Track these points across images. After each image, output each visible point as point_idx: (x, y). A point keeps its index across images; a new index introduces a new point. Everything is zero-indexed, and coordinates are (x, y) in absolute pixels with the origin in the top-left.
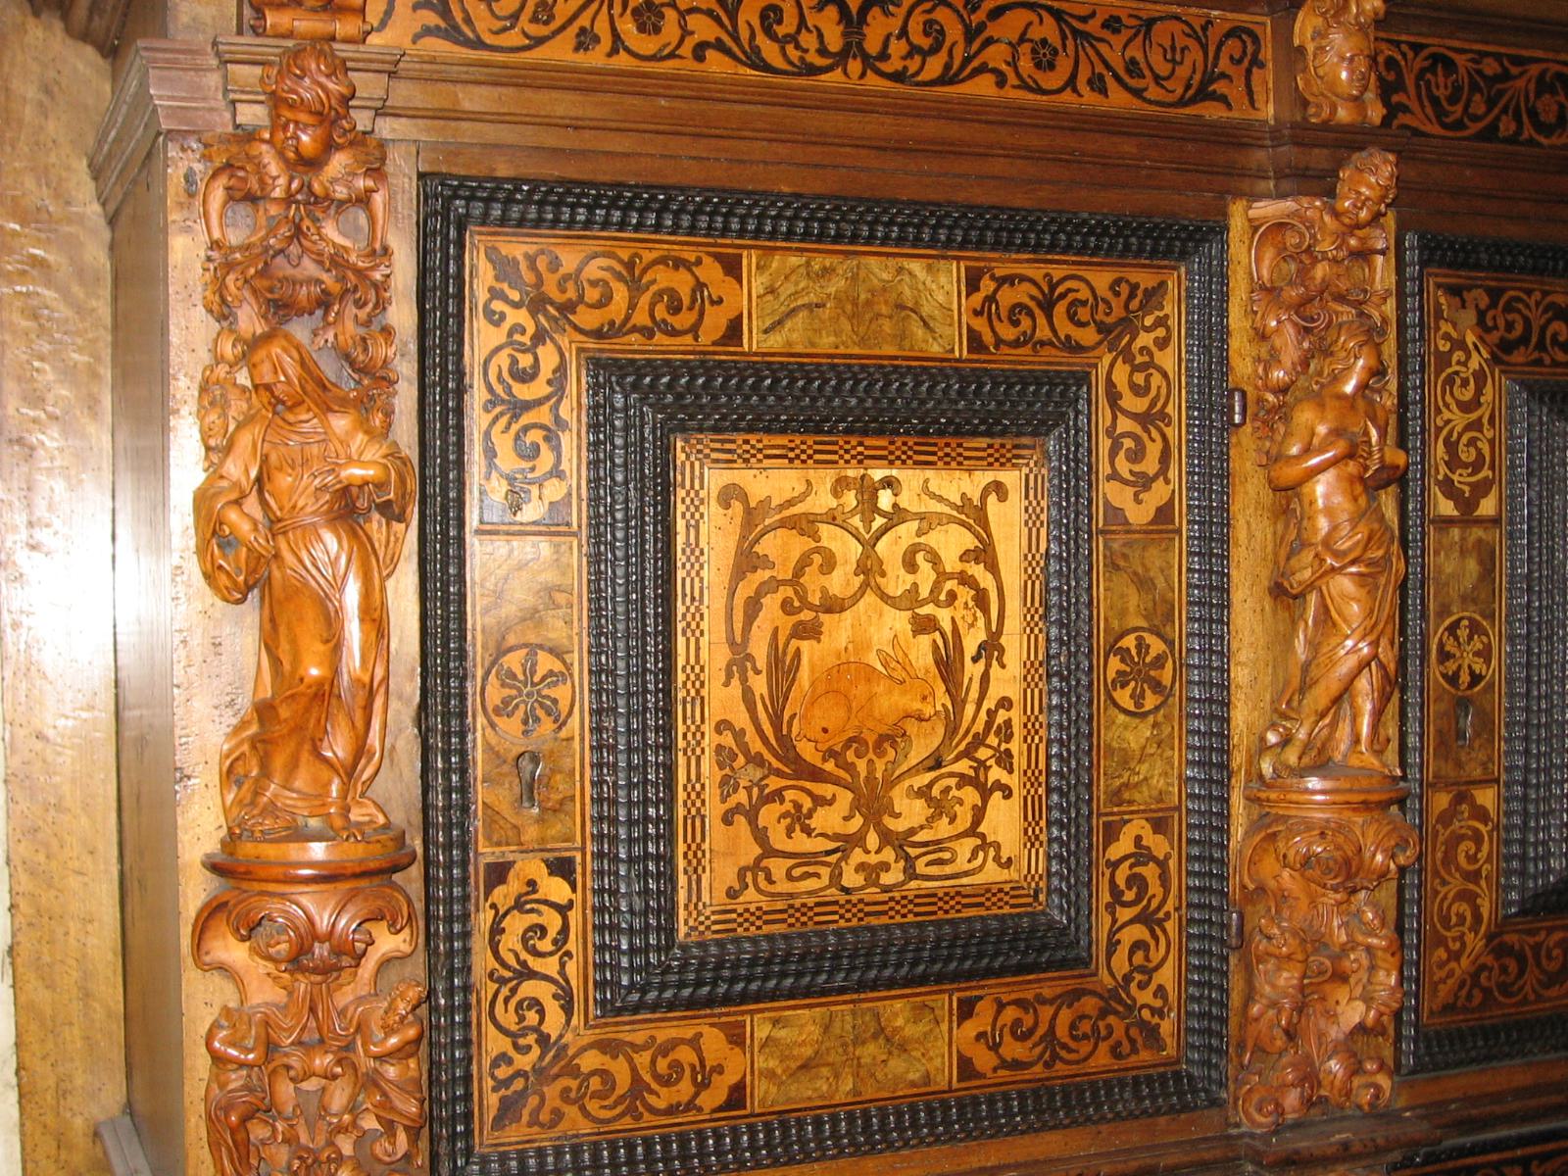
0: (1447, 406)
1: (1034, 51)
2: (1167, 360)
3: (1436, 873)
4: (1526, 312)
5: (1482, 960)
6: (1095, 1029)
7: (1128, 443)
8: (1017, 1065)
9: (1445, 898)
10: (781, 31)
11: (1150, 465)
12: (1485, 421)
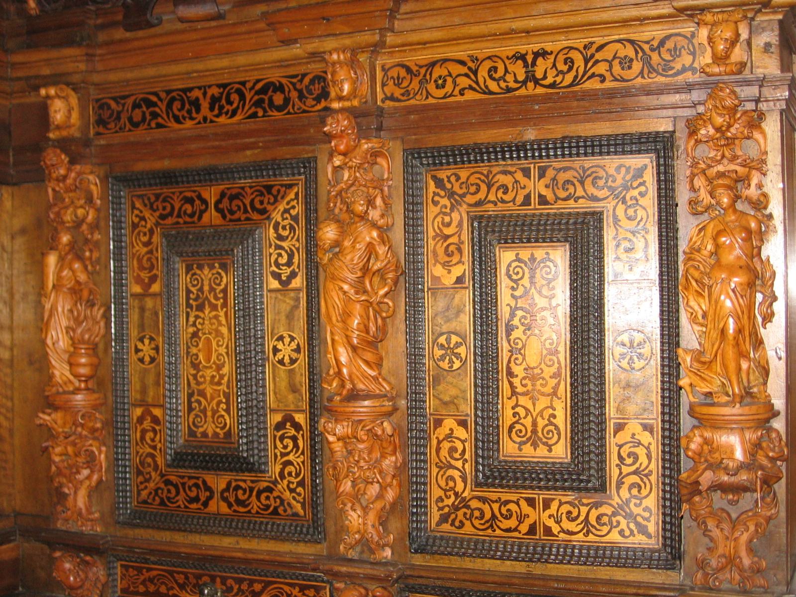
0: (298, 464)
1: (620, 63)
2: (437, 493)
3: (298, 249)
4: (258, 504)
5: (273, 207)
6: (468, 188)
7: (457, 456)
8: (505, 173)
9: (292, 238)
10: (497, 76)
11: (446, 445)
12: (279, 457)
